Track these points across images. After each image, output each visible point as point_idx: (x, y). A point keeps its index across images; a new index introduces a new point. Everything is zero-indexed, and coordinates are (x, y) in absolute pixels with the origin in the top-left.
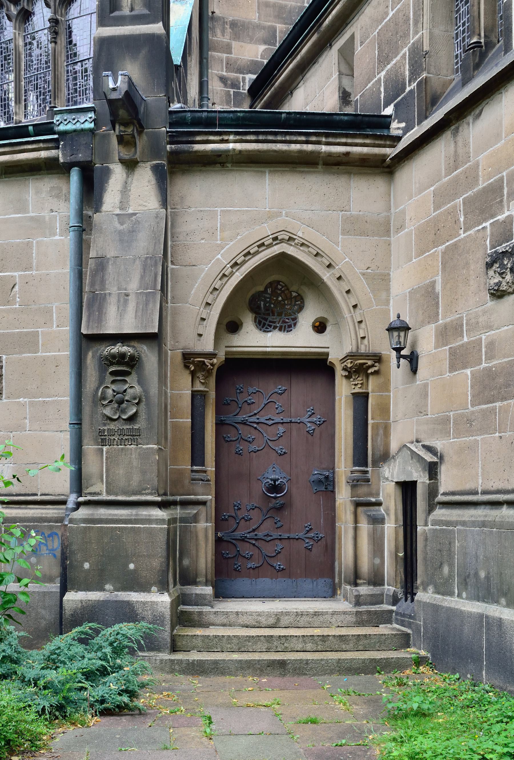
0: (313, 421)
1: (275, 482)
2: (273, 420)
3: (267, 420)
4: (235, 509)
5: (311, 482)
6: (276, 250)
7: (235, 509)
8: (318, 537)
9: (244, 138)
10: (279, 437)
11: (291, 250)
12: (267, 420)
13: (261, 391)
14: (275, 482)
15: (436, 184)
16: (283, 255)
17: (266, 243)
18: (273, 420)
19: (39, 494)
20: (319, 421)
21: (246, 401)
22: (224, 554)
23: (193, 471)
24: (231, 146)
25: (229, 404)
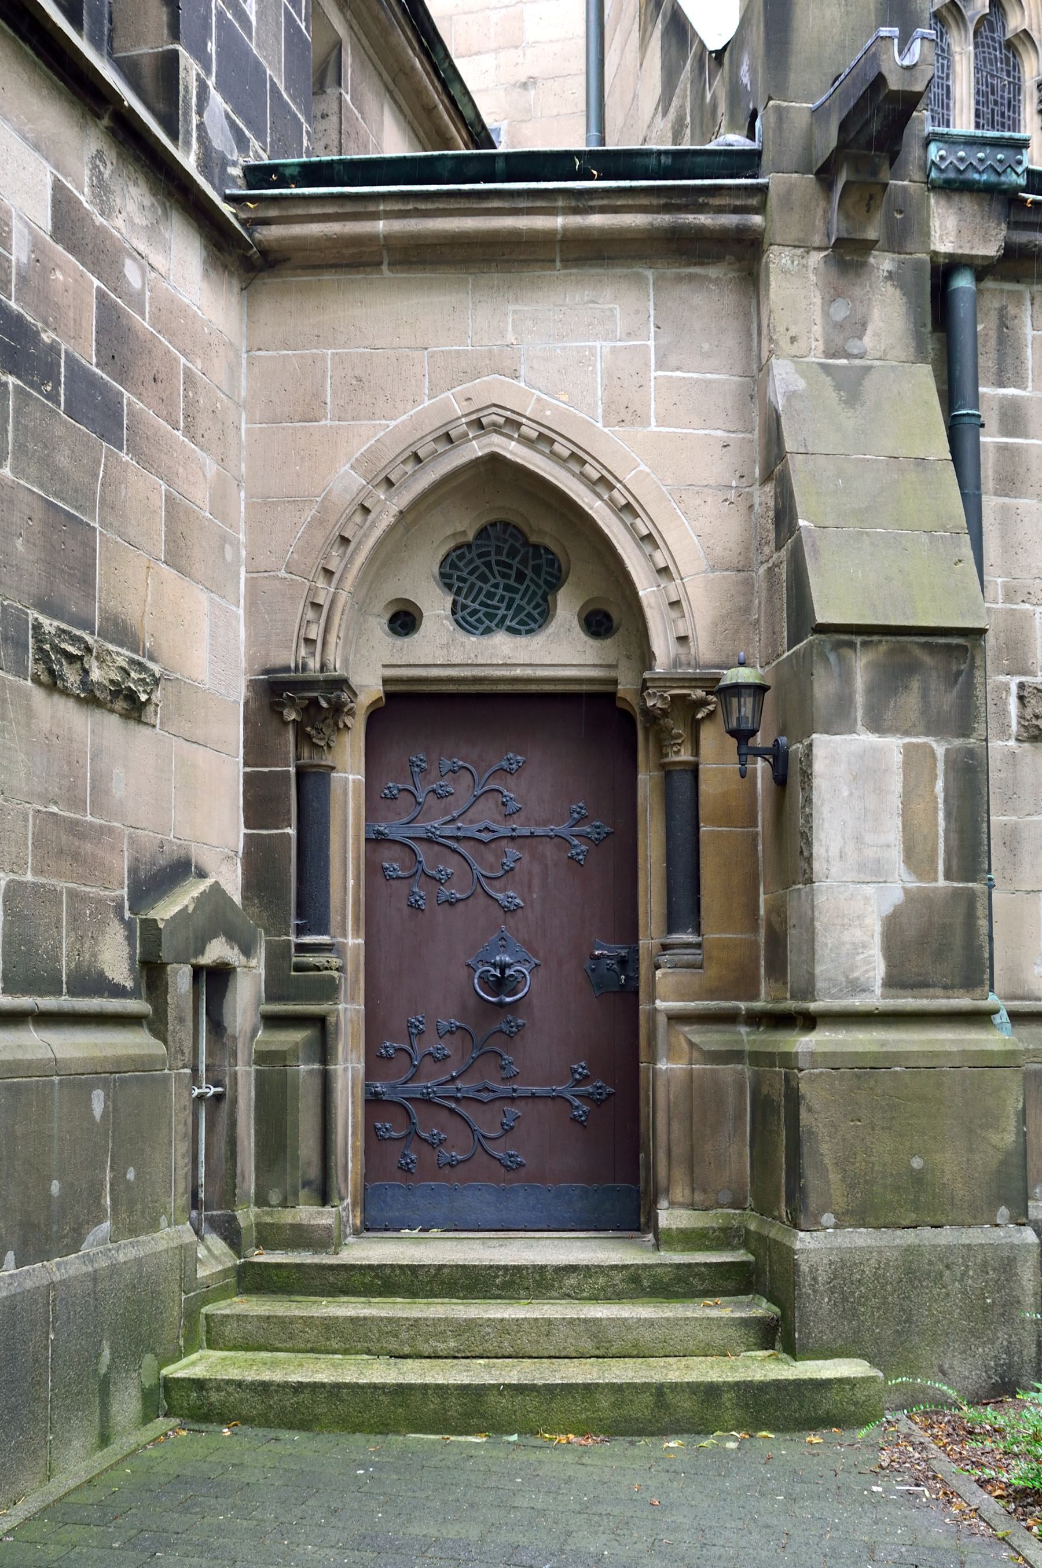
0: (584, 833)
1: (502, 972)
2: (493, 831)
3: (479, 831)
4: (410, 1034)
5: (589, 971)
6: (477, 448)
7: (410, 1034)
8: (600, 1094)
9: (422, 206)
10: (507, 872)
11: (513, 450)
12: (479, 831)
13: (470, 767)
14: (502, 972)
15: (423, 207)
16: (494, 459)
17: (557, 447)
18: (493, 831)
19: (1001, 1018)
20: (598, 834)
21: (434, 791)
22: (380, 1129)
23: (302, 948)
24: (381, 226)
25: (394, 798)
